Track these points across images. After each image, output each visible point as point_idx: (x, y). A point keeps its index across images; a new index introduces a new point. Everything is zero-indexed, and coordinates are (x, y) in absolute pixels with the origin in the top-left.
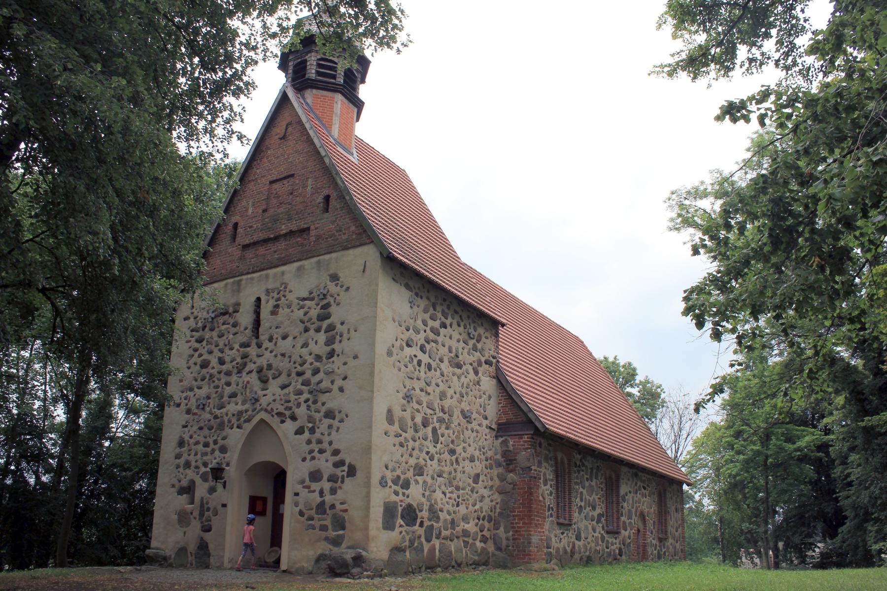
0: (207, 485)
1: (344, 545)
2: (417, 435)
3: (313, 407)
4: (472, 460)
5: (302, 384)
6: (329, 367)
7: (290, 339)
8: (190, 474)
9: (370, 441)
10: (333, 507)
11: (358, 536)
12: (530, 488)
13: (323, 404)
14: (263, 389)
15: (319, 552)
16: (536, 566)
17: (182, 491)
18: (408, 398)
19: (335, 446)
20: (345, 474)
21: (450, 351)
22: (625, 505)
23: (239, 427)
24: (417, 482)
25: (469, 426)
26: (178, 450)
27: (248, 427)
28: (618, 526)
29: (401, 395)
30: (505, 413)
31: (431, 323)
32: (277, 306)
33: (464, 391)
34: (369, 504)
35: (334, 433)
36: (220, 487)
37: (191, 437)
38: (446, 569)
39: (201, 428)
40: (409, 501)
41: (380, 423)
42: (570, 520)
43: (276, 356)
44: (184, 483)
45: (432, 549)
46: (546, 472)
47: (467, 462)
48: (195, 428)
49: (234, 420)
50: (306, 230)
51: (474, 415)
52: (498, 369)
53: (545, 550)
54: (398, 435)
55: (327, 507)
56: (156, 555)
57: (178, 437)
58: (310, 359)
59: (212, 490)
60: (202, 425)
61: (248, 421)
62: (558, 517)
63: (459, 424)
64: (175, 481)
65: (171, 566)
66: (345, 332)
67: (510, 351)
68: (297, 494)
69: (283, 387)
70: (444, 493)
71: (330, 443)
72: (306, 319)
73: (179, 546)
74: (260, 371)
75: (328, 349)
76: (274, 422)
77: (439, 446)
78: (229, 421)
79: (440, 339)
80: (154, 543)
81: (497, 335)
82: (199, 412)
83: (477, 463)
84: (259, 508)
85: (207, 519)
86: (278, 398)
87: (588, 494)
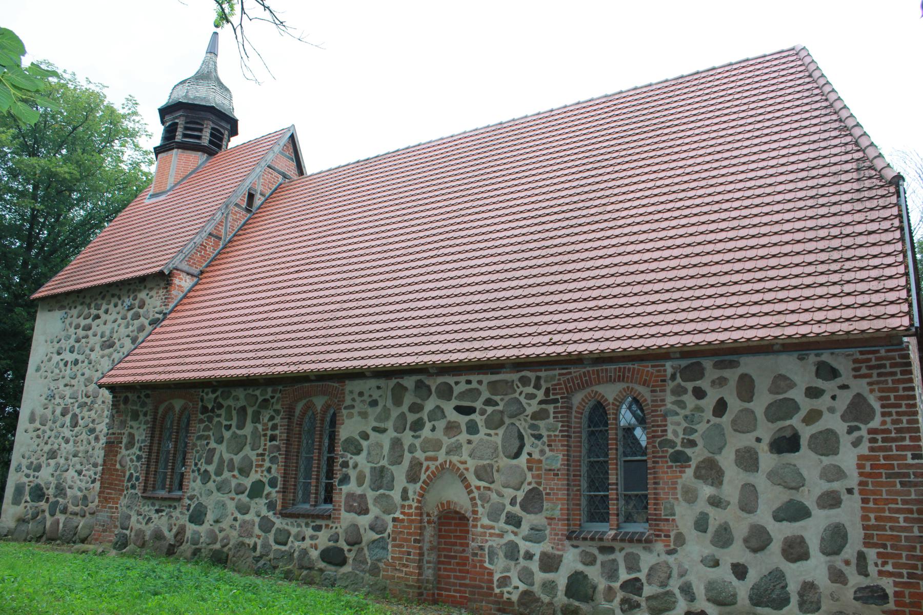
40: (39, 481)
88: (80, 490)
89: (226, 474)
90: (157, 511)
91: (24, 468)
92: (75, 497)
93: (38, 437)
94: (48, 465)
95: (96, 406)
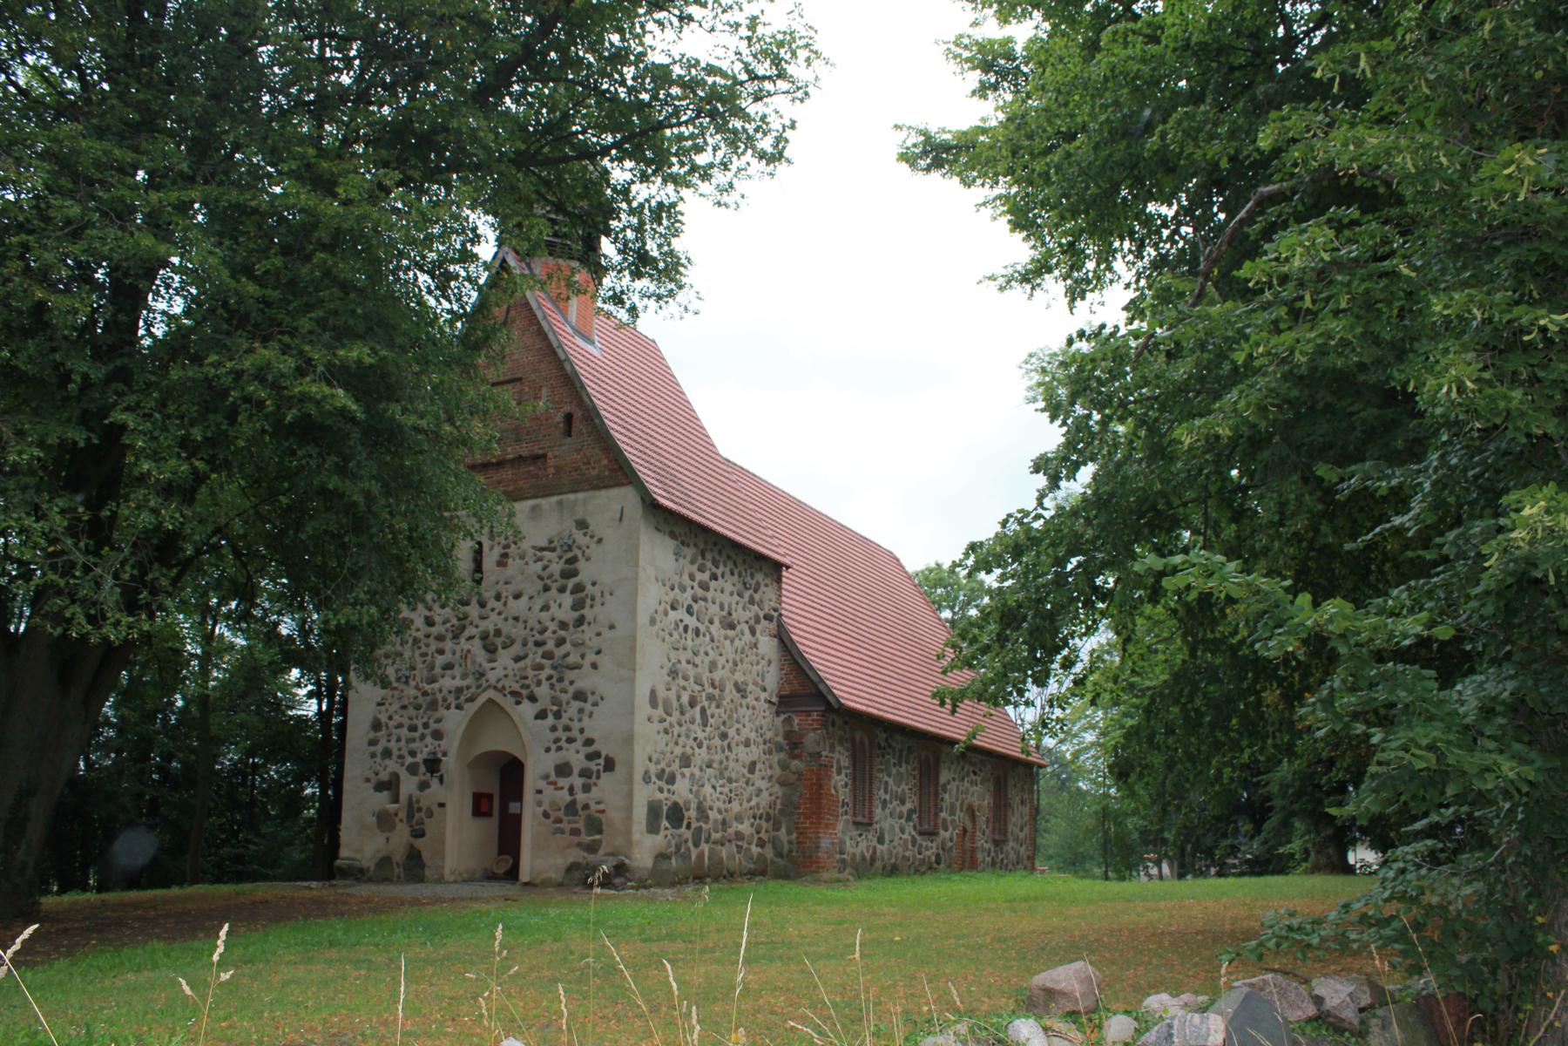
0: (416, 780)
1: (601, 852)
2: (683, 719)
3: (558, 686)
4: (747, 744)
5: (543, 657)
6: (578, 637)
7: (525, 599)
8: (392, 765)
9: (632, 730)
10: (586, 807)
11: (619, 841)
12: (819, 779)
13: (572, 683)
14: (491, 661)
15: (571, 860)
16: (826, 875)
17: (380, 787)
18: (673, 673)
19: (587, 734)
21: (722, 609)
22: (946, 796)
23: (458, 707)
24: (683, 775)
25: (744, 702)
26: (372, 735)
27: (471, 708)
28: (936, 825)
29: (666, 670)
30: (788, 682)
31: (699, 576)
32: (505, 555)
34: (630, 802)
35: (586, 718)
36: (435, 783)
37: (390, 718)
38: (716, 879)
39: (404, 707)
40: (675, 798)
41: (643, 708)
42: (871, 818)
43: (506, 619)
44: (384, 776)
45: (701, 856)
46: (841, 757)
47: (741, 747)
48: (396, 706)
49: (451, 699)
50: (539, 458)
51: (750, 688)
52: (780, 625)
53: (838, 856)
54: (662, 721)
55: (579, 807)
56: (351, 867)
57: (371, 717)
58: (552, 626)
59: (424, 786)
60: (406, 702)
61: (471, 700)
62: (855, 815)
64: (370, 774)
65: (370, 880)
66: (598, 595)
67: (797, 601)
68: (539, 792)
69: (517, 659)
70: (714, 787)
71: (582, 731)
72: (545, 574)
73: (380, 855)
74: (484, 637)
75: (576, 614)
76: (507, 702)
77: (708, 729)
78: (445, 700)
79: (709, 595)
80: (344, 852)
81: (779, 580)
82: (401, 686)
83: (753, 747)
84: (484, 808)
85: (418, 820)
86: (511, 673)
87: (895, 785)
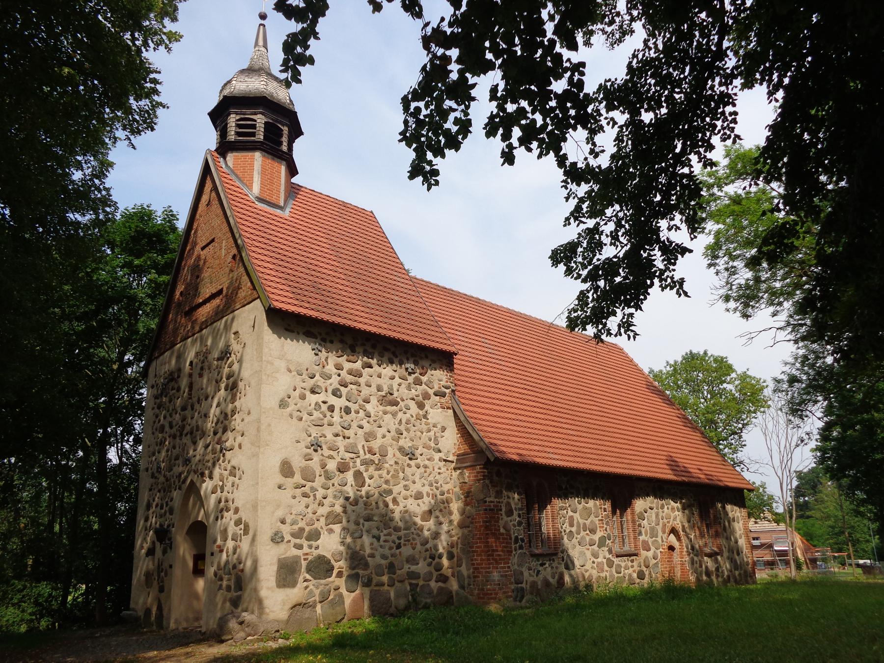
20: (242, 532)
22: (645, 523)
25: (413, 463)
29: (302, 445)
33: (402, 428)
40: (320, 552)
47: (411, 501)
63: (396, 463)
79: (362, 380)
88: (384, 557)
89: (583, 533)
90: (542, 565)
91: (287, 537)
92: (379, 566)
93: (305, 495)
94: (331, 531)
95: (386, 465)
